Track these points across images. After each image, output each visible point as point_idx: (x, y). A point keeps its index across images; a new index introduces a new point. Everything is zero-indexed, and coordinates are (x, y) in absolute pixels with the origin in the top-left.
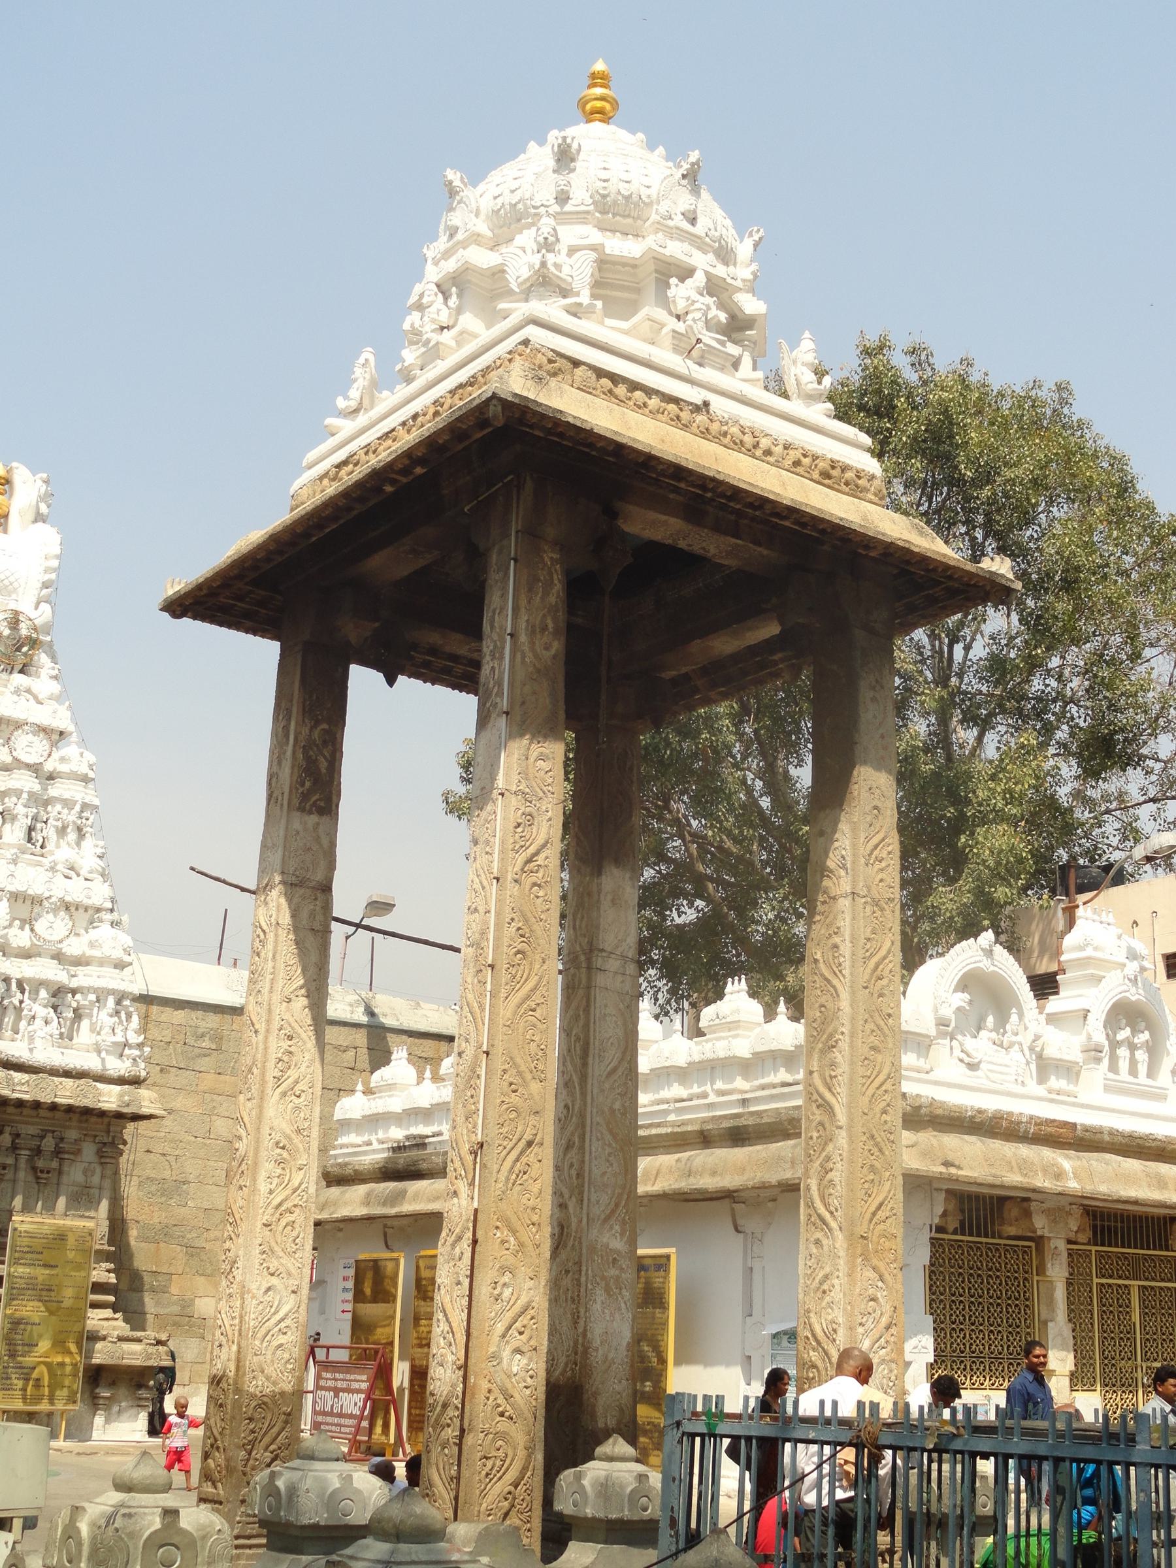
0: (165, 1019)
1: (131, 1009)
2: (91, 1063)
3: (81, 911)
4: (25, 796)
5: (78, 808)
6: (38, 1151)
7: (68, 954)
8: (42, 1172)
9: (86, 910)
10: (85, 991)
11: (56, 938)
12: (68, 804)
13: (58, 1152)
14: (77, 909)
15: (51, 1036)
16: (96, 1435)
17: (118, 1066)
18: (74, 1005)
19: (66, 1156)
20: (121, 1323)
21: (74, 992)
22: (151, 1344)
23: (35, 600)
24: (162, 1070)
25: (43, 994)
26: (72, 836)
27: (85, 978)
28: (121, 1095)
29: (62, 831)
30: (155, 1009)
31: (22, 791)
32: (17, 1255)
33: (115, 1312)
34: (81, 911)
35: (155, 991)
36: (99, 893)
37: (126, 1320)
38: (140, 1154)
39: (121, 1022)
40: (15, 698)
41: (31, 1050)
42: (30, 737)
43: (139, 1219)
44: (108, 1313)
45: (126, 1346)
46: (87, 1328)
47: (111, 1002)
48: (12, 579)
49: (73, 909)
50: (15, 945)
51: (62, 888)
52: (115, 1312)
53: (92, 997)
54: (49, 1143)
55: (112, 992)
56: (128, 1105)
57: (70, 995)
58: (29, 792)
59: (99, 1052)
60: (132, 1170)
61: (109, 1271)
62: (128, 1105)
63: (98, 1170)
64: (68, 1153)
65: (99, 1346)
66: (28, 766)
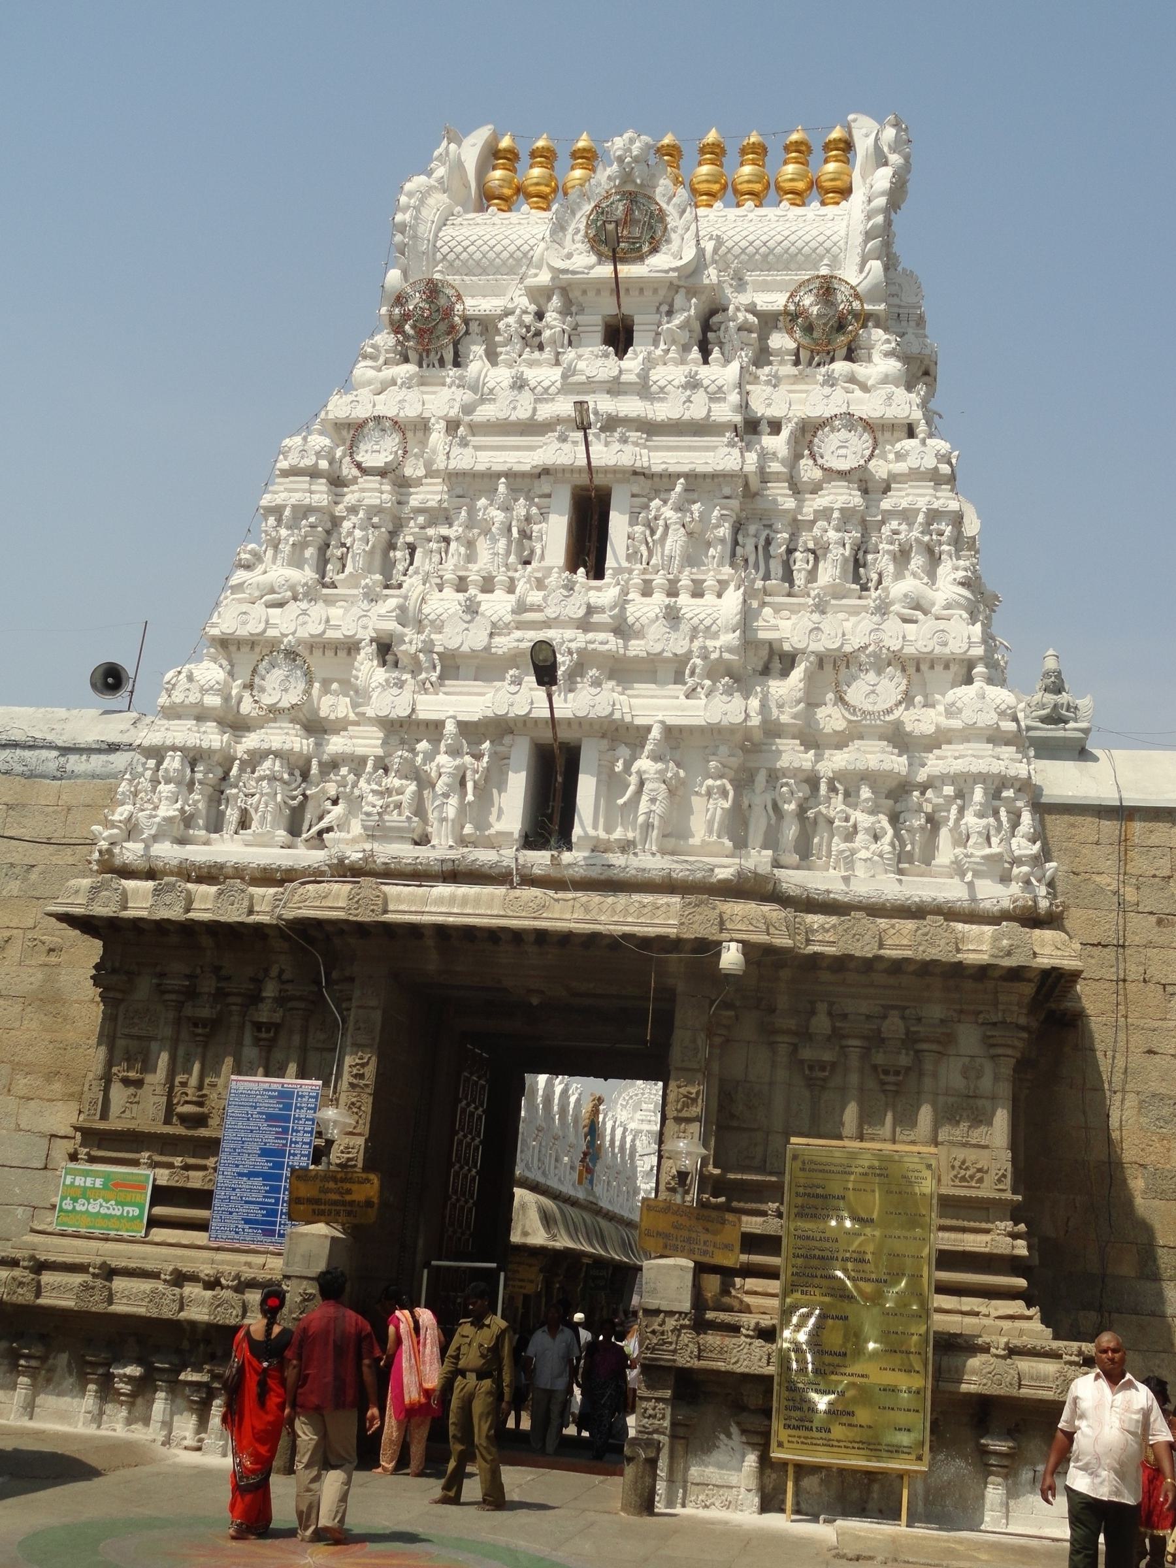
0: (1157, 842)
1: (1020, 804)
2: (952, 891)
3: (939, 668)
4: (836, 514)
5: (921, 518)
6: (876, 1040)
7: (917, 733)
8: (886, 1072)
9: (947, 667)
10: (938, 783)
11: (882, 706)
12: (907, 516)
13: (910, 1040)
14: (932, 667)
15: (881, 856)
16: (991, 1519)
17: (995, 894)
18: (928, 808)
19: (925, 1046)
20: (1036, 1325)
21: (924, 788)
22: (1071, 1363)
23: (858, 259)
24: (1160, 922)
25: (865, 793)
26: (917, 561)
27: (935, 764)
28: (996, 939)
29: (902, 557)
30: (1137, 827)
31: (832, 509)
32: (799, 1201)
33: (1029, 1306)
34: (939, 668)
35: (1134, 797)
36: (964, 636)
37: (1045, 1321)
38: (1137, 1059)
39: (999, 828)
40: (827, 390)
41: (846, 880)
42: (844, 434)
43: (1147, 1161)
44: (1017, 1307)
45: (1024, 1365)
46: (935, 1328)
47: (978, 794)
48: (828, 244)
49: (924, 667)
50: (828, 730)
51: (895, 635)
52: (1029, 1306)
53: (949, 790)
54: (894, 1026)
55: (981, 778)
56: (1009, 954)
57: (916, 793)
58: (842, 510)
59: (962, 875)
60: (1125, 1082)
61: (1015, 1236)
62: (1009, 954)
63: (988, 1068)
64: (927, 1040)
65: (974, 1362)
66: (843, 475)
